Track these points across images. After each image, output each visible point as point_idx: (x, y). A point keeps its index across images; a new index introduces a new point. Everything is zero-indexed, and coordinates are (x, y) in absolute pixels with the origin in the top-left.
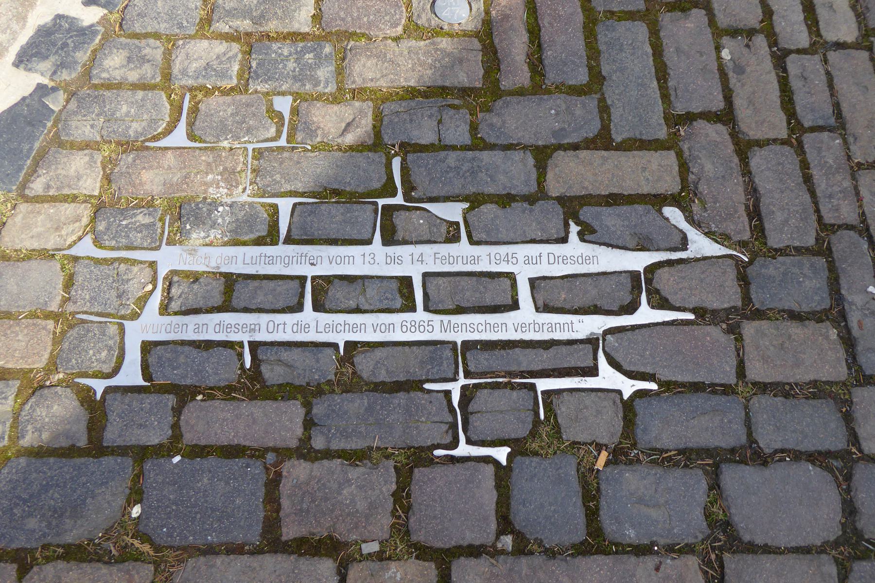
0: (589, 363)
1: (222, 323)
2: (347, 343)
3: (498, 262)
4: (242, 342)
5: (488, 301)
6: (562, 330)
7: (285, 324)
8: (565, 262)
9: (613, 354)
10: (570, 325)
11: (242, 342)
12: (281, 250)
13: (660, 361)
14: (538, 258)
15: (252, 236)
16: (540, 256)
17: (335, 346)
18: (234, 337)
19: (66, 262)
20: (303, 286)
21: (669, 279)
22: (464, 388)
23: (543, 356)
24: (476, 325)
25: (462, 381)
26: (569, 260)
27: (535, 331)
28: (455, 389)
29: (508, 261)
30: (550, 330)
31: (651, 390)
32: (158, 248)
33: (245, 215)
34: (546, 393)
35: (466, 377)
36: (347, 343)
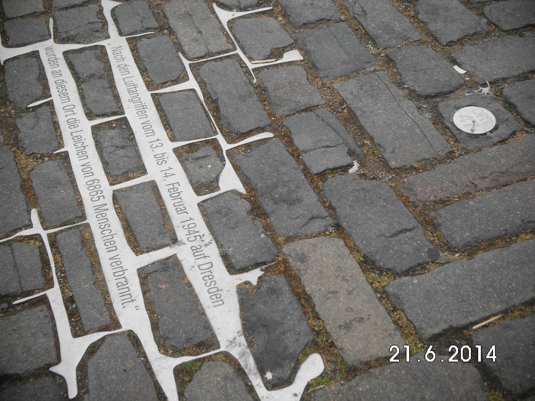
0: (87, 325)
1: (65, 83)
2: (67, 152)
3: (186, 227)
4: (51, 96)
5: (137, 229)
6: (121, 295)
7: (74, 114)
8: (207, 278)
9: (103, 347)
10: (130, 300)
11: (51, 96)
12: (146, 96)
13: (107, 392)
14: (203, 256)
15: (212, 16)
16: (205, 257)
17: (61, 145)
18: (53, 90)
19: (418, 342)
20: (114, 114)
21: (218, 376)
22: (37, 237)
23: (87, 284)
24: (109, 228)
25: (44, 234)
26: (209, 281)
27: (114, 273)
28: (37, 229)
29: (190, 234)
30: (119, 284)
31: (67, 392)
32: (121, 34)
33: (525, 31)
34: (44, 300)
35: (49, 235)
36: (67, 152)
